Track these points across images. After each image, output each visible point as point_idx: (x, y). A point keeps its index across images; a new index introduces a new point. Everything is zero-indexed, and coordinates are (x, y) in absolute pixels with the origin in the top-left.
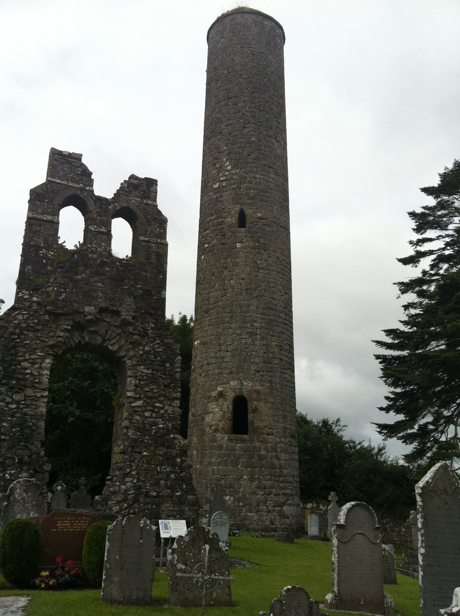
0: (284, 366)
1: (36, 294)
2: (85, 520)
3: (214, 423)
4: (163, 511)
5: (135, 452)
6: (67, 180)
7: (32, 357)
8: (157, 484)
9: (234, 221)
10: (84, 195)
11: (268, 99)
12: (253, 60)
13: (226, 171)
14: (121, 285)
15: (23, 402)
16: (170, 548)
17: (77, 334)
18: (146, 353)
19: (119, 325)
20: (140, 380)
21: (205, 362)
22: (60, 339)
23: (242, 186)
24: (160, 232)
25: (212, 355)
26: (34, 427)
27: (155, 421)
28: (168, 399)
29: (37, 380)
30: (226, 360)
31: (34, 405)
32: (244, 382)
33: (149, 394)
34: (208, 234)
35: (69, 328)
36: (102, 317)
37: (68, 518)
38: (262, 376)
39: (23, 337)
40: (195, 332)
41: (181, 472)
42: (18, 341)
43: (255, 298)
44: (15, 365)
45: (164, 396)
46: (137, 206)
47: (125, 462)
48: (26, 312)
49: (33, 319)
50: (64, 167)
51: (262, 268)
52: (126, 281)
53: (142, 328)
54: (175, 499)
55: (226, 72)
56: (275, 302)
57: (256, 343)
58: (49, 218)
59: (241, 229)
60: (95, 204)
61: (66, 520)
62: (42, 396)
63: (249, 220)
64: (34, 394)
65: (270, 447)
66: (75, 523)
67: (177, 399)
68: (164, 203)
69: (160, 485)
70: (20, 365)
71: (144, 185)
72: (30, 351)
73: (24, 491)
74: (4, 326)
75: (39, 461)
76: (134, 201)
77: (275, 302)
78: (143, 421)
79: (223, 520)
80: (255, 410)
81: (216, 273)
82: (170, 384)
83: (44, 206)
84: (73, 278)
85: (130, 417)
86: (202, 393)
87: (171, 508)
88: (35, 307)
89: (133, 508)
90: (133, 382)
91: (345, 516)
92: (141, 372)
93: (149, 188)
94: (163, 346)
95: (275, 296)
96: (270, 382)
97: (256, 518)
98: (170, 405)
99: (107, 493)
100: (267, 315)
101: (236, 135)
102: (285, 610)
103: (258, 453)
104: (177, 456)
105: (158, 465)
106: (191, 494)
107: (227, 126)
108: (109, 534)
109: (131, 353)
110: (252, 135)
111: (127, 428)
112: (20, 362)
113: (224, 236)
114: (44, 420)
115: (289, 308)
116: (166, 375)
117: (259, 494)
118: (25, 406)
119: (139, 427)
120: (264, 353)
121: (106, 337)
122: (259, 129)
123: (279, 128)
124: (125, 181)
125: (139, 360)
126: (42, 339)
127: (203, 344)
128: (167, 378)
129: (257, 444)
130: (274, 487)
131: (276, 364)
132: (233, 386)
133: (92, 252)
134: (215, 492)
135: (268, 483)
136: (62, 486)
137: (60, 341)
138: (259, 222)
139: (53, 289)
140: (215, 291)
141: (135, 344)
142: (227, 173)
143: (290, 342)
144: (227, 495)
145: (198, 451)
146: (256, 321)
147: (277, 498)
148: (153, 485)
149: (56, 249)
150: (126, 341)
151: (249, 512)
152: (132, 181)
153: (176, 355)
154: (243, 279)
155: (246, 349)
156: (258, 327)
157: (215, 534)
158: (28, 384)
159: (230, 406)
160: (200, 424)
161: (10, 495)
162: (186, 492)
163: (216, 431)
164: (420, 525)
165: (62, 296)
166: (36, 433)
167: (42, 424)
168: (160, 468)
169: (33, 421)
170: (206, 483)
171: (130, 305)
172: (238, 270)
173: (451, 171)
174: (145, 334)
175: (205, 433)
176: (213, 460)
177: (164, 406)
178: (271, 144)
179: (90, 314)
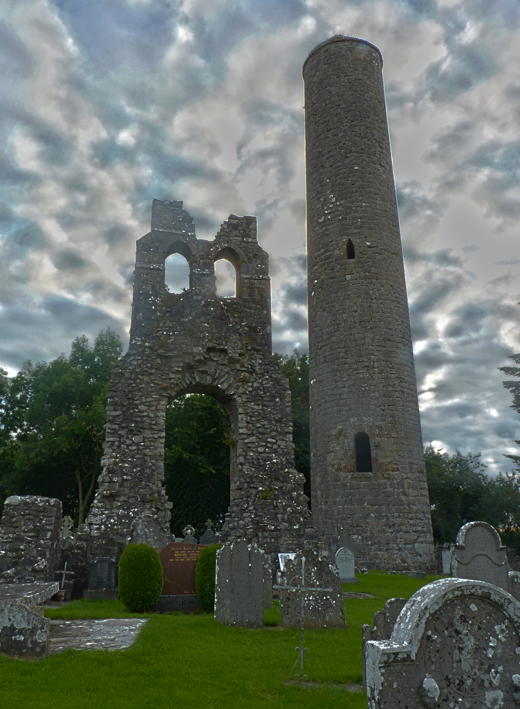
0: (406, 398)
3: (336, 462)
4: (282, 545)
6: (170, 228)
7: (148, 400)
8: (275, 517)
9: (342, 253)
11: (369, 125)
12: (350, 88)
13: (330, 204)
14: (227, 324)
15: (142, 444)
17: (187, 375)
18: (255, 390)
19: (227, 364)
20: (251, 417)
21: (322, 400)
22: (172, 381)
24: (261, 269)
25: (330, 392)
26: (153, 467)
27: (268, 456)
28: (281, 434)
29: (154, 422)
30: (344, 396)
32: (364, 418)
33: (260, 430)
34: (316, 270)
36: (210, 357)
37: (184, 549)
38: (383, 410)
39: (138, 381)
40: (311, 371)
42: (134, 385)
44: (133, 408)
46: (237, 245)
47: (242, 498)
48: (140, 358)
49: (147, 363)
51: (375, 298)
52: (231, 319)
53: (250, 364)
54: (293, 532)
55: (323, 105)
56: (392, 332)
57: (374, 376)
59: (350, 260)
61: (183, 550)
62: (160, 437)
63: (357, 251)
64: (152, 436)
65: (397, 483)
66: (191, 553)
67: (289, 433)
68: (265, 242)
69: (277, 519)
70: (137, 409)
71: (244, 224)
72: (145, 395)
73: (146, 527)
74: (120, 373)
75: (161, 500)
76: (235, 241)
77: (392, 332)
79: (347, 556)
80: (377, 447)
81: (327, 309)
83: (150, 255)
84: (180, 321)
85: (244, 454)
87: (290, 542)
88: (147, 351)
90: (244, 419)
91: (464, 536)
93: (249, 226)
94: (272, 381)
95: (391, 326)
96: (393, 416)
97: (386, 556)
98: (282, 440)
99: (227, 529)
100: (384, 347)
101: (338, 167)
102: (389, 623)
103: (384, 491)
104: (294, 490)
105: (273, 500)
106: (309, 527)
107: (328, 159)
109: (241, 390)
110: (355, 164)
111: (242, 464)
112: (137, 405)
113: (333, 269)
114: (162, 460)
115: (407, 338)
116: (277, 410)
118: (144, 447)
119: (253, 464)
120: (384, 386)
121: (215, 376)
122: (361, 156)
123: (383, 153)
124: (225, 222)
125: (248, 396)
126: (155, 382)
127: (318, 382)
128: (278, 413)
129: (383, 481)
130: (403, 524)
131: (398, 397)
132: (353, 423)
133: (196, 294)
134: (341, 531)
135: (397, 521)
136: (191, 529)
137: (173, 383)
138: (369, 251)
139: (163, 333)
140: (327, 327)
141: (244, 381)
143: (411, 373)
144: (355, 534)
145: (322, 491)
146: (372, 354)
147: (408, 536)
148: (270, 520)
149: (163, 295)
150: (235, 378)
151: (378, 551)
152: (232, 221)
153: (285, 389)
155: (364, 384)
156: (375, 360)
158: (145, 427)
159: (352, 443)
160: (322, 464)
163: (339, 470)
165: (171, 339)
166: (156, 473)
167: (162, 464)
169: (153, 461)
170: (333, 523)
171: (235, 342)
172: (350, 303)
174: (253, 371)
176: (338, 500)
177: (277, 441)
178: (376, 170)
179: (198, 354)
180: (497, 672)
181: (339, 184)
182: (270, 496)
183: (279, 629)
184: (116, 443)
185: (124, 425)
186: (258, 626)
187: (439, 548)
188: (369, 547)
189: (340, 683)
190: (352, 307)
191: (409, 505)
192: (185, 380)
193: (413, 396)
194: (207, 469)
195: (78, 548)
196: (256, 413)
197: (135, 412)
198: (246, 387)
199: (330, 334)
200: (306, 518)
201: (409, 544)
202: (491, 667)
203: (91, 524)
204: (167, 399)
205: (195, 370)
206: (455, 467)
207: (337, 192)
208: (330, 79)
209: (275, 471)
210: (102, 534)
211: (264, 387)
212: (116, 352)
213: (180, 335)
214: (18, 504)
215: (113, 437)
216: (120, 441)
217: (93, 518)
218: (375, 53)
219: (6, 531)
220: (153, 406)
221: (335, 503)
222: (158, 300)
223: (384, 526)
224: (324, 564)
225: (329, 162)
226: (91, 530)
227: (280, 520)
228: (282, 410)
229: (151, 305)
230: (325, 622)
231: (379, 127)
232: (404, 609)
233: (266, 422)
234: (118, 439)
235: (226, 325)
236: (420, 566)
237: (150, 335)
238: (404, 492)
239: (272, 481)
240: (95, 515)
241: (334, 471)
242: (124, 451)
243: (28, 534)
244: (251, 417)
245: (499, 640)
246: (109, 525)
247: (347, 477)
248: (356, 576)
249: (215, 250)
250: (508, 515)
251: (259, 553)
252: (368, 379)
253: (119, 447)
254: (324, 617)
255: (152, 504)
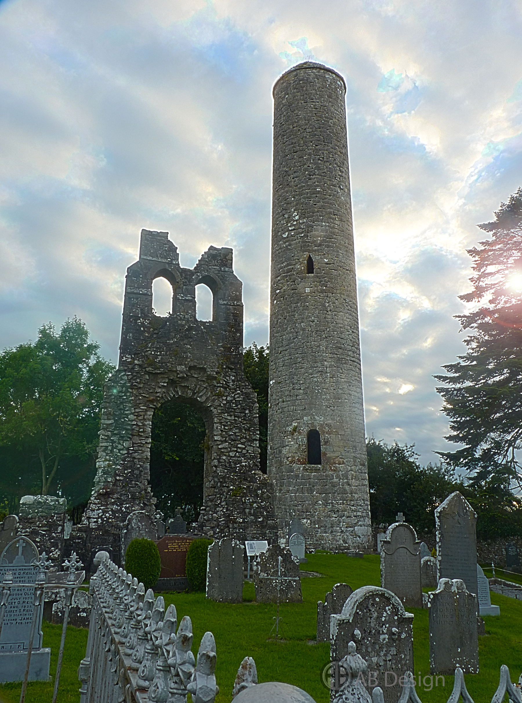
0: (353, 400)
1: (138, 357)
2: (189, 543)
5: (223, 486)
8: (243, 512)
10: (171, 268)
11: (331, 150)
15: (132, 448)
16: (255, 561)
17: (171, 389)
20: (225, 426)
21: (280, 400)
22: (158, 394)
23: (309, 234)
25: (287, 393)
26: (141, 469)
31: (140, 450)
34: (279, 280)
35: (166, 385)
36: (192, 374)
39: (128, 394)
41: (262, 502)
42: (125, 397)
43: (324, 338)
44: (124, 418)
45: (246, 438)
46: (216, 274)
49: (136, 379)
50: (154, 245)
53: (225, 381)
55: (291, 127)
56: (344, 341)
58: (144, 291)
60: (181, 275)
61: (175, 543)
62: (146, 443)
63: (316, 266)
65: (342, 475)
69: (245, 513)
70: (127, 418)
76: (214, 270)
77: (344, 341)
78: (229, 460)
79: (299, 540)
82: (250, 428)
85: (218, 457)
86: (279, 428)
88: (137, 368)
89: (224, 533)
92: (225, 418)
95: (343, 336)
98: (251, 446)
100: (336, 354)
106: (271, 520)
107: (293, 179)
108: (209, 552)
109: (217, 403)
110: (317, 186)
111: (216, 466)
113: (294, 281)
115: (356, 346)
116: (246, 420)
117: (333, 517)
119: (225, 466)
130: (346, 510)
133: (181, 319)
134: (293, 517)
135: (341, 507)
136: (160, 514)
137: (159, 397)
140: (287, 334)
141: (220, 395)
142: (295, 223)
143: (358, 377)
144: (304, 518)
149: (150, 317)
150: (212, 393)
151: (324, 533)
154: (313, 321)
156: (328, 366)
157: (288, 550)
161: (128, 524)
162: (266, 518)
164: (438, 540)
168: (245, 499)
169: (140, 463)
170: (285, 509)
171: (213, 362)
172: (308, 313)
173: (509, 206)
175: (282, 464)
177: (246, 447)
179: (182, 372)
180: (386, 627)
181: (302, 203)
182: (239, 494)
183: (254, 603)
184: (110, 448)
185: (116, 432)
186: (239, 602)
187: (375, 528)
188: (316, 530)
189: (302, 640)
190: (310, 317)
191: (351, 494)
192: (169, 394)
193: (359, 398)
194: (171, 456)
195: (79, 538)
196: (229, 423)
197: (125, 420)
198: (221, 400)
199: (289, 340)
200: (268, 512)
201: (351, 527)
202: (383, 625)
203: (89, 518)
204: (153, 410)
205: (178, 385)
206: (393, 456)
207: (300, 211)
208: (298, 103)
209: (244, 473)
210: (99, 526)
211: (236, 401)
212: (82, 339)
213: (166, 355)
214: (32, 503)
215: (106, 442)
216: (112, 445)
217: (91, 512)
218: (339, 81)
219: (23, 526)
220: (141, 415)
221: (288, 491)
222: (147, 322)
223: (329, 511)
224: (288, 555)
225: (294, 182)
226: (89, 523)
227: (247, 514)
228: (250, 420)
229: (140, 327)
230: (288, 599)
231: (340, 151)
232: (348, 600)
233: (237, 431)
234: (111, 444)
235: (206, 347)
236: (359, 546)
237: (139, 353)
238: (348, 482)
239: (241, 481)
240: (93, 510)
241: (288, 463)
242: (116, 455)
243: (42, 529)
244: (225, 426)
245: (387, 613)
246: (105, 519)
247: (300, 469)
248: (305, 557)
249: (196, 278)
250: (436, 500)
251: (240, 548)
252: (321, 382)
253: (112, 451)
254: (287, 594)
255: (140, 500)
